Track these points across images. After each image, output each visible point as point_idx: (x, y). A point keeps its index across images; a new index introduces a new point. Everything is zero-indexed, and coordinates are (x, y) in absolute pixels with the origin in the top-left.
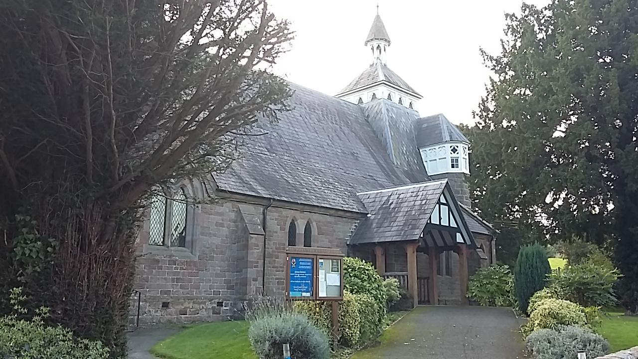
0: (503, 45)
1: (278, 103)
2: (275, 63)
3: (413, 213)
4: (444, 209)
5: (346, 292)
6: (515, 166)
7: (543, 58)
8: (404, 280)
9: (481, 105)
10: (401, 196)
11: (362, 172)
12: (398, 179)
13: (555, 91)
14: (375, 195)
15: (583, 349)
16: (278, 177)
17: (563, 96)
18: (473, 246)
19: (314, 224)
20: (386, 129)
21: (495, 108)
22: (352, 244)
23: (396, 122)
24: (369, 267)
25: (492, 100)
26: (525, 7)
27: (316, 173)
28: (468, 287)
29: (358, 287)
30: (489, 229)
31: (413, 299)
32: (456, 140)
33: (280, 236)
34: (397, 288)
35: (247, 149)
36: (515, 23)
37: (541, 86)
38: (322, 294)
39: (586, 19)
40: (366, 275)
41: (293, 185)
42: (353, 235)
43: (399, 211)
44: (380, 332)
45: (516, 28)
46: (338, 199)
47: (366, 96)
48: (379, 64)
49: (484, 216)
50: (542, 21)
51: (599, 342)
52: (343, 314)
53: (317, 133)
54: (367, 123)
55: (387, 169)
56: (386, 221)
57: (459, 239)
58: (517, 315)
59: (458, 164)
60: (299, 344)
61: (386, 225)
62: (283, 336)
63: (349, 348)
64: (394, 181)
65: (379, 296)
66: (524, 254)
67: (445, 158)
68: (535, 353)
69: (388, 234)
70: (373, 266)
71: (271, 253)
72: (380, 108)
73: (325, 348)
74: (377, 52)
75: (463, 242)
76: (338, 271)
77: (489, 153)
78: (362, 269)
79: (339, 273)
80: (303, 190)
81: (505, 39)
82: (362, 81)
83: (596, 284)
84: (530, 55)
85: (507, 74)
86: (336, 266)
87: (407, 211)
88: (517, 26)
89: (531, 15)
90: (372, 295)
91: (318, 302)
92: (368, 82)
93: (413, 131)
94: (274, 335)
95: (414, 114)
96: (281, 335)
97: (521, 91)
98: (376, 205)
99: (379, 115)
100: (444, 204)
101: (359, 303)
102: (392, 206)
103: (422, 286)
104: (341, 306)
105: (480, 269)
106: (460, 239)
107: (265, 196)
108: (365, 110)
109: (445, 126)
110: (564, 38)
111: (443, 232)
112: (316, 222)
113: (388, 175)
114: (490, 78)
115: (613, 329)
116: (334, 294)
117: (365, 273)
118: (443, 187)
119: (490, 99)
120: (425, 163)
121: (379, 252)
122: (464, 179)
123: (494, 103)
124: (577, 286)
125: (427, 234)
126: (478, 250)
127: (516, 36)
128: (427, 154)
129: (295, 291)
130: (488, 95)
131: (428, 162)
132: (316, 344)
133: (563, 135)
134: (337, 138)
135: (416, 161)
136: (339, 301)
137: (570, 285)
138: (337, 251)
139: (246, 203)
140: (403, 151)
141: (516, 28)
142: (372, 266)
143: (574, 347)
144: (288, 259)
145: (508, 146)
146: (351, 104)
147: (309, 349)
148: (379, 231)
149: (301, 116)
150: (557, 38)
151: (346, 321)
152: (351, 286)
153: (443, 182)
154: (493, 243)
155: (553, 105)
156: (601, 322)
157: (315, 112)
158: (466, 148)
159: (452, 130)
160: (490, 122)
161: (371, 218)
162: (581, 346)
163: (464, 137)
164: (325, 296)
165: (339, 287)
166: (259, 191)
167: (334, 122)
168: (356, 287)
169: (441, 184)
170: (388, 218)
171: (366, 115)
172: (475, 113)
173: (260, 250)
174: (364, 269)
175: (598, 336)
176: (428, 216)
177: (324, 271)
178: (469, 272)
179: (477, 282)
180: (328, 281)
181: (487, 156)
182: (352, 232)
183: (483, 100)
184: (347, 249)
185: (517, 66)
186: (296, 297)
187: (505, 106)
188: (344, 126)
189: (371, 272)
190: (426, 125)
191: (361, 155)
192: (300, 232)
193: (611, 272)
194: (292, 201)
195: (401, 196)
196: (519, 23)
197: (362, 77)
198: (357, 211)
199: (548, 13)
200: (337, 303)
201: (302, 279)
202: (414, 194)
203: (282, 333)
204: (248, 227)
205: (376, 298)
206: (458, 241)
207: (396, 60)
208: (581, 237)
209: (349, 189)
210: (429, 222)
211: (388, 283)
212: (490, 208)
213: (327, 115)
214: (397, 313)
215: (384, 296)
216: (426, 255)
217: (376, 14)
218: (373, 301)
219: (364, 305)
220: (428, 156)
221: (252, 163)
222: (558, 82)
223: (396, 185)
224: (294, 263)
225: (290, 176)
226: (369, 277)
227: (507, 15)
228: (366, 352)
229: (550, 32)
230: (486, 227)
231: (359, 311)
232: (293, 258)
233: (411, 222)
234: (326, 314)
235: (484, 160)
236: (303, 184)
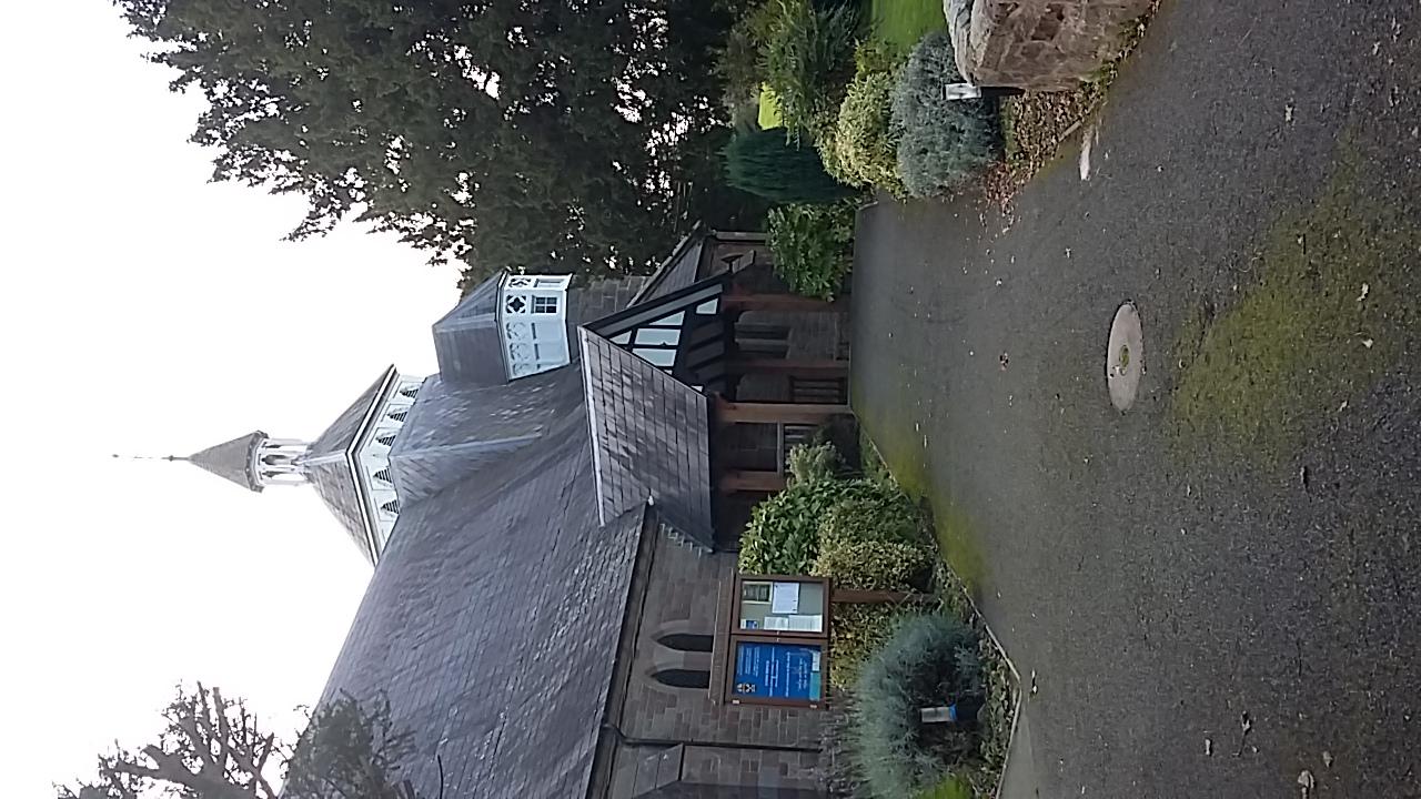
0: (288, 188)
1: (370, 730)
2: (272, 736)
4: (643, 336)
5: (814, 570)
6: (558, 183)
7: (323, 107)
8: (795, 432)
9: (419, 244)
10: (612, 428)
11: (554, 511)
12: (574, 431)
13: (398, 88)
14: (606, 486)
15: (940, 87)
16: (554, 707)
17: (409, 73)
18: (727, 280)
19: (664, 626)
21: (428, 214)
22: (712, 542)
23: (446, 428)
24: (761, 514)
25: (408, 220)
26: (202, 137)
28: (812, 297)
29: (804, 541)
30: (690, 244)
32: (494, 299)
33: (689, 703)
34: (811, 450)
35: (485, 780)
36: (239, 161)
37: (384, 115)
38: (816, 624)
39: (240, 12)
40: (779, 522)
41: (574, 672)
42: (692, 538)
43: (643, 436)
44: (903, 497)
45: (249, 159)
46: (611, 570)
47: (381, 494)
48: (308, 462)
49: (666, 252)
50: (239, 102)
51: (927, 53)
52: (861, 580)
53: (459, 612)
54: (444, 493)
56: (665, 466)
57: (709, 308)
58: (872, 202)
60: (922, 684)
61: (672, 465)
62: (904, 722)
63: (934, 567)
64: (578, 441)
65: (825, 494)
66: (744, 179)
67: (533, 324)
68: (946, 183)
70: (761, 504)
71: (725, 730)
72: (409, 463)
73: (934, 627)
74: (278, 466)
75: (716, 301)
76: (768, 586)
77: (526, 234)
78: (766, 530)
79: (771, 583)
80: (586, 649)
81: (271, 183)
82: (343, 502)
83: (809, 45)
84: (312, 133)
85: (352, 185)
86: (757, 590)
87: (645, 417)
88: (245, 157)
89: (222, 125)
90: (822, 510)
91: (834, 634)
92: (344, 492)
93: (467, 392)
94: (902, 742)
95: (431, 388)
96: (901, 726)
97: (393, 158)
98: (628, 483)
100: (633, 337)
101: (839, 542)
102: (633, 449)
104: (843, 582)
105: (775, 267)
106: (711, 307)
107: (596, 742)
109: (462, 321)
110: (280, 61)
111: (694, 342)
112: (659, 623)
113: (565, 454)
114: (297, 234)
115: (903, 14)
116: (817, 596)
117: (774, 523)
118: (596, 336)
119: (407, 224)
120: (541, 370)
121: (731, 483)
122: (581, 289)
123: (418, 216)
124: (812, 83)
125: (697, 376)
126: (734, 270)
127: (268, 161)
128: (522, 363)
129: (808, 688)
130: (397, 227)
131: (539, 361)
132: (924, 647)
133: (496, 78)
134: (473, 564)
136: (832, 587)
137: (809, 97)
138: (723, 586)
139: (608, 788)
140: (514, 417)
141: (249, 159)
142: (759, 507)
143: (935, 103)
144: (738, 702)
145: (513, 193)
146: (397, 529)
147: (935, 662)
148: (686, 480)
149: (415, 648)
150: (278, 76)
151: (876, 572)
152: (802, 557)
153: (584, 337)
154: (720, 235)
155: (428, 95)
156: (886, 43)
157: (409, 614)
158: (514, 280)
159: (472, 307)
160: (457, 228)
161: (657, 497)
162: (934, 90)
163: (490, 281)
164: (821, 617)
165: (803, 585)
166: (582, 756)
168: (805, 545)
170: (659, 461)
171: (424, 494)
172: (436, 258)
173: (718, 756)
174: (766, 525)
175: (914, 54)
176: (657, 372)
177: (766, 618)
178: (780, 293)
179: (802, 275)
180: (788, 610)
181: (534, 238)
182: (685, 541)
183: (406, 239)
184: (722, 554)
185: (335, 162)
186: (822, 687)
187: (424, 196)
188: (446, 548)
189: (773, 510)
191: (515, 511)
192: (682, 659)
193: (785, 12)
194: (609, 678)
195: (612, 428)
196: (238, 152)
197: (334, 500)
199: (221, 89)
200: (837, 592)
201: (783, 667)
202: (609, 399)
203: (898, 723)
204: (665, 783)
205: (828, 503)
206: (714, 312)
207: (302, 418)
208: (715, 57)
209: (589, 543)
210: (670, 372)
211: (799, 469)
212: (647, 237)
213: (419, 586)
214: (863, 453)
215: (826, 484)
216: (742, 381)
218: (834, 510)
219: (843, 531)
220: (526, 361)
221: (517, 771)
222: (377, 80)
223: (588, 436)
224: (746, 688)
225: (553, 680)
226: (783, 515)
227: (218, 177)
228: (942, 532)
229: (264, 88)
231: (854, 541)
232: (734, 690)
233: (671, 411)
234: (860, 615)
235: (539, 246)
236: (573, 648)
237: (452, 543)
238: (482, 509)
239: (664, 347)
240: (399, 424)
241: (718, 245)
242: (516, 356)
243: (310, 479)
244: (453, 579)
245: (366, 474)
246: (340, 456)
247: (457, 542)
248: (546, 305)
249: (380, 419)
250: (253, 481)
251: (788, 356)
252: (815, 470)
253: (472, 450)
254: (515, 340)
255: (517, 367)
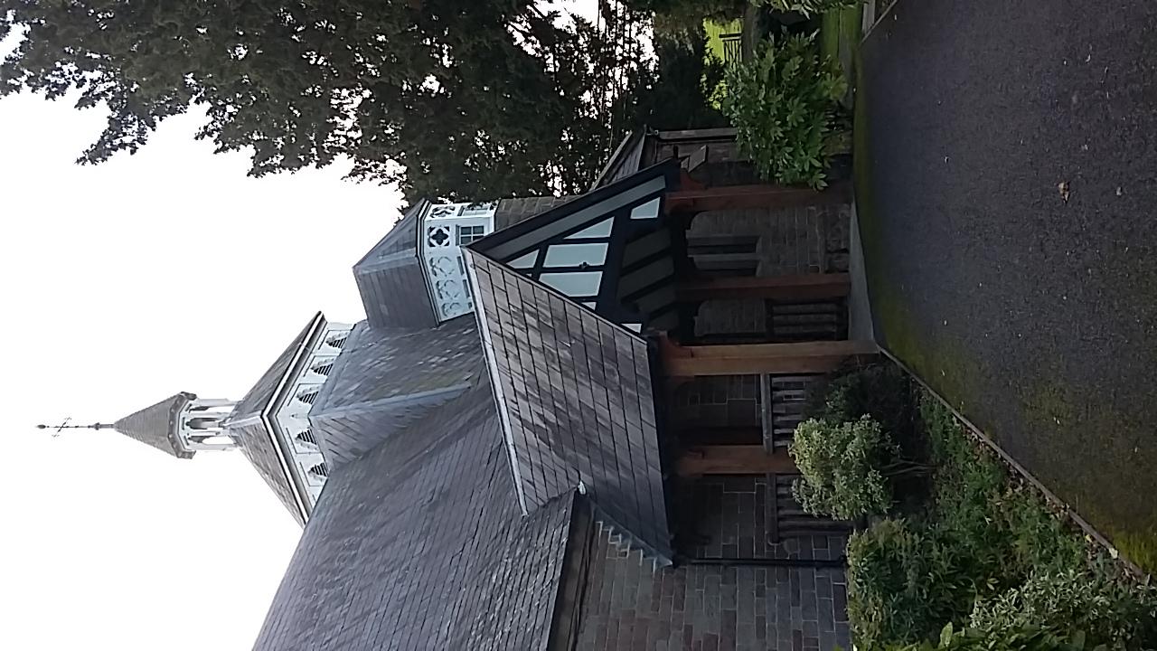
3: (564, 353)
4: (555, 255)
8: (788, 386)
10: (521, 388)
20: (384, 408)
27: (463, 640)
28: (795, 184)
31: (852, 356)
47: (307, 457)
55: (479, 408)
57: (649, 211)
59: (474, 227)
61: (606, 440)
69: (635, 436)
81: (74, 93)
82: (270, 467)
92: (269, 453)
95: (359, 337)
99: (350, 425)
100: (541, 259)
102: (552, 418)
103: (791, 318)
108: (340, 460)
121: (694, 465)
134: (389, 548)
135: (469, 331)
140: (442, 365)
154: (664, 135)
158: (436, 210)
167: (353, 552)
169: (474, 266)
171: (351, 456)
190: (384, 308)
195: (521, 388)
198: (566, 528)
207: (227, 379)
209: (510, 538)
210: (592, 305)
217: (93, 429)
220: (456, 300)
223: (494, 408)
230: (625, 155)
233: (596, 363)
237: (374, 517)
238: (406, 476)
239: (586, 268)
240: (323, 378)
241: (662, 146)
242: (444, 295)
243: (238, 442)
244: (368, 567)
245: (287, 436)
246: (255, 419)
247: (377, 518)
248: (472, 235)
249: (303, 373)
250: (178, 447)
251: (757, 274)
252: (846, 468)
253: (398, 405)
254: (441, 277)
255: (447, 307)
